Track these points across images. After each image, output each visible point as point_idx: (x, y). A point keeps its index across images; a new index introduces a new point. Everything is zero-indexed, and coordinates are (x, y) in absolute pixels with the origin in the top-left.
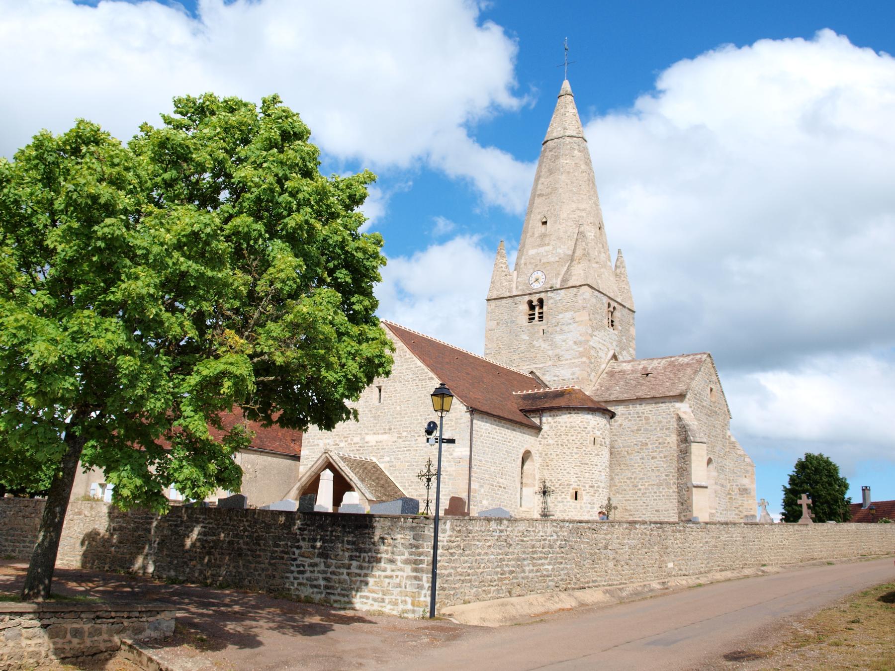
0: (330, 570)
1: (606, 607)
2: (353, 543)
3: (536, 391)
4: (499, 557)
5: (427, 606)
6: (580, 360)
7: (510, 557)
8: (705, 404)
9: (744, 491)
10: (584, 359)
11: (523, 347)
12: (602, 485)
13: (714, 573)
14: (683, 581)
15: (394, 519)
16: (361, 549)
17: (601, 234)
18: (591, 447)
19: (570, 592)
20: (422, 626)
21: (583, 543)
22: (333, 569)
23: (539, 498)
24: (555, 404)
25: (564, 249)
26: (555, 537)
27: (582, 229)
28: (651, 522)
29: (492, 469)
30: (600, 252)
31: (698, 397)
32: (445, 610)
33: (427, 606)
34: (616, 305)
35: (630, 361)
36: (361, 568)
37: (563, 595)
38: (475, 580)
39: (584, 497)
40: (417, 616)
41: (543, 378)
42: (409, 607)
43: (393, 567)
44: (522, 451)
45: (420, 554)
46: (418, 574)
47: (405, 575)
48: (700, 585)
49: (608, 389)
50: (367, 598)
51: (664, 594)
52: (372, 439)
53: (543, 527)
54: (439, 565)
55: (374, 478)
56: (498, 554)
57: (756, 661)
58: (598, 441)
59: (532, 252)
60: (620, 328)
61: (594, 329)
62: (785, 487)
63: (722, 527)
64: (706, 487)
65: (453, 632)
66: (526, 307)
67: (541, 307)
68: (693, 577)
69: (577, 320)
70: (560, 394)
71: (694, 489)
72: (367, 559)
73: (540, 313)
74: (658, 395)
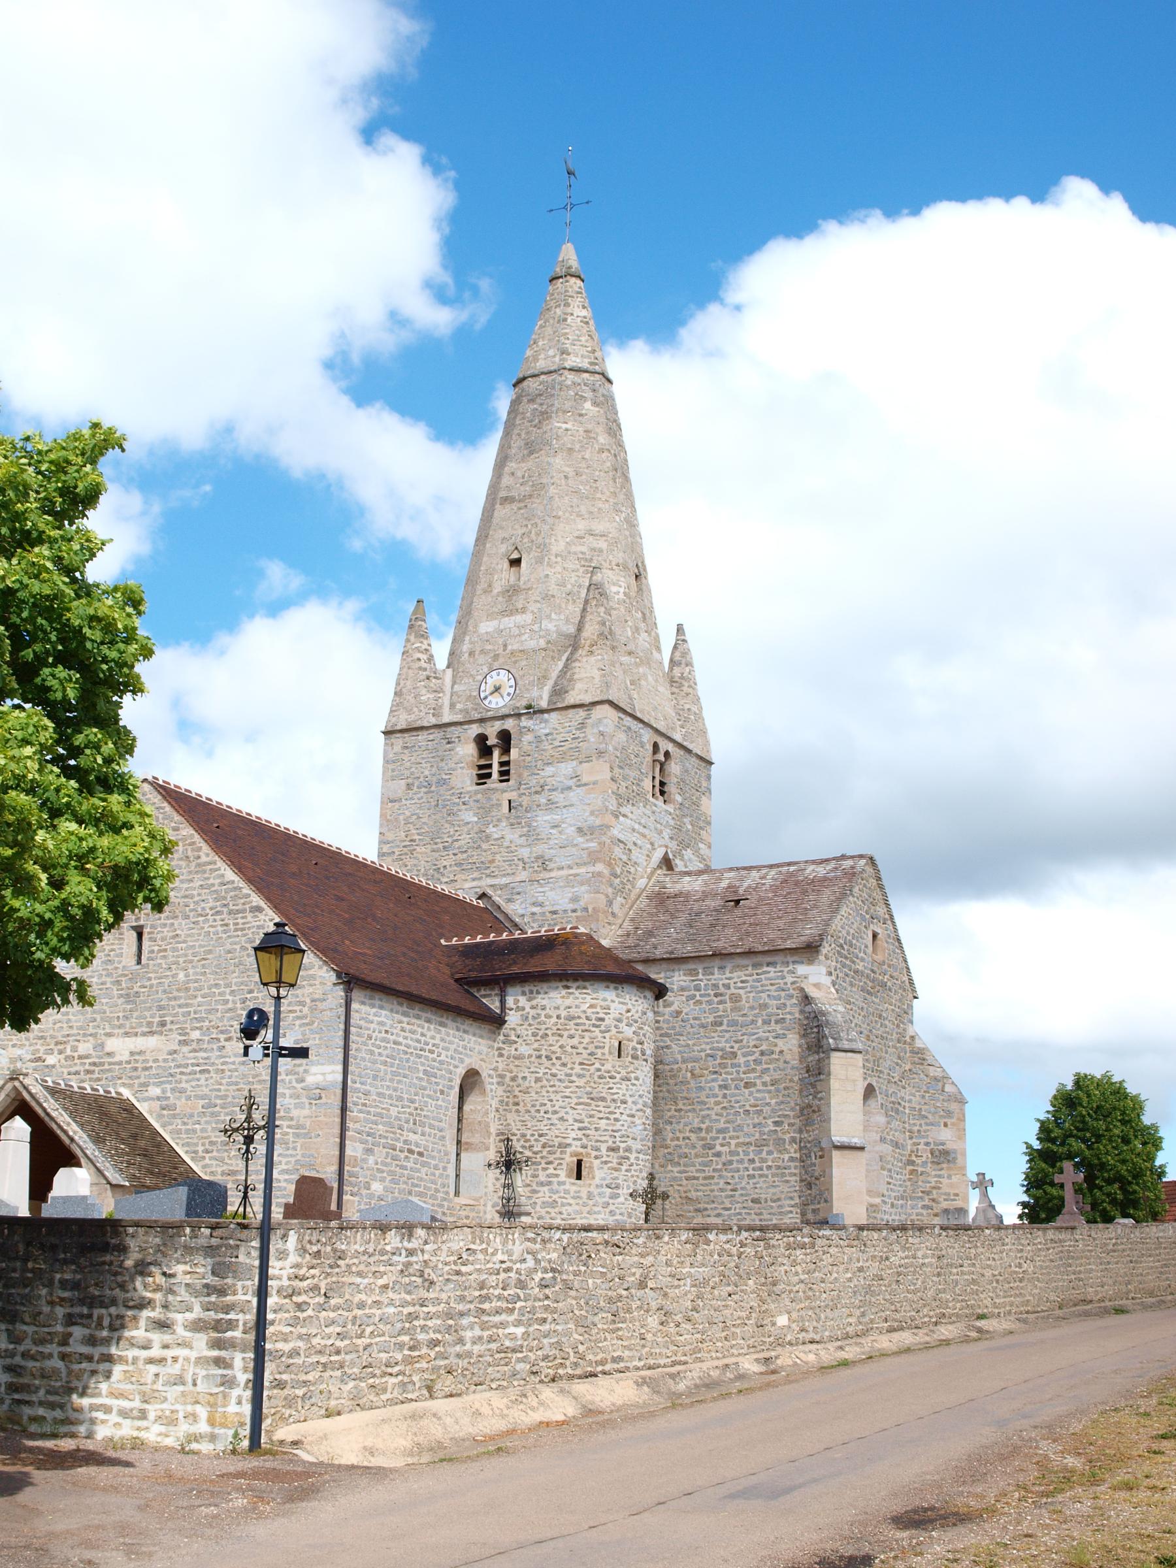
0: (21, 1348)
1: (641, 1416)
2: (76, 1286)
3: (492, 937)
4: (406, 1311)
6: (591, 869)
10: (600, 867)
11: (465, 840)
12: (637, 1146)
13: (874, 1336)
14: (810, 1356)
15: (169, 1229)
16: (94, 1297)
17: (640, 590)
18: (611, 1063)
19: (563, 1384)
20: (232, 1469)
21: (592, 1275)
22: (27, 1345)
23: (493, 1180)
24: (534, 965)
25: (558, 623)
26: (530, 1263)
27: (598, 577)
29: (394, 1111)
30: (637, 630)
31: (846, 952)
32: (285, 1433)
33: (242, 1424)
34: (670, 747)
35: (700, 873)
38: (353, 1364)
39: (598, 1173)
40: (220, 1447)
41: (509, 908)
42: (203, 1427)
44: (461, 1070)
45: (227, 1309)
46: (223, 1353)
47: (193, 1355)
48: (844, 1364)
49: (650, 934)
51: (768, 1385)
54: (270, 1330)
55: (124, 1135)
57: (961, 1529)
58: (628, 1047)
60: (679, 798)
62: (1029, 1146)
64: (862, 1148)
65: (302, 1482)
66: (468, 750)
67: (506, 748)
68: (831, 1346)
69: (585, 780)
70: (545, 945)
71: (836, 1154)
73: (502, 764)
74: (761, 949)
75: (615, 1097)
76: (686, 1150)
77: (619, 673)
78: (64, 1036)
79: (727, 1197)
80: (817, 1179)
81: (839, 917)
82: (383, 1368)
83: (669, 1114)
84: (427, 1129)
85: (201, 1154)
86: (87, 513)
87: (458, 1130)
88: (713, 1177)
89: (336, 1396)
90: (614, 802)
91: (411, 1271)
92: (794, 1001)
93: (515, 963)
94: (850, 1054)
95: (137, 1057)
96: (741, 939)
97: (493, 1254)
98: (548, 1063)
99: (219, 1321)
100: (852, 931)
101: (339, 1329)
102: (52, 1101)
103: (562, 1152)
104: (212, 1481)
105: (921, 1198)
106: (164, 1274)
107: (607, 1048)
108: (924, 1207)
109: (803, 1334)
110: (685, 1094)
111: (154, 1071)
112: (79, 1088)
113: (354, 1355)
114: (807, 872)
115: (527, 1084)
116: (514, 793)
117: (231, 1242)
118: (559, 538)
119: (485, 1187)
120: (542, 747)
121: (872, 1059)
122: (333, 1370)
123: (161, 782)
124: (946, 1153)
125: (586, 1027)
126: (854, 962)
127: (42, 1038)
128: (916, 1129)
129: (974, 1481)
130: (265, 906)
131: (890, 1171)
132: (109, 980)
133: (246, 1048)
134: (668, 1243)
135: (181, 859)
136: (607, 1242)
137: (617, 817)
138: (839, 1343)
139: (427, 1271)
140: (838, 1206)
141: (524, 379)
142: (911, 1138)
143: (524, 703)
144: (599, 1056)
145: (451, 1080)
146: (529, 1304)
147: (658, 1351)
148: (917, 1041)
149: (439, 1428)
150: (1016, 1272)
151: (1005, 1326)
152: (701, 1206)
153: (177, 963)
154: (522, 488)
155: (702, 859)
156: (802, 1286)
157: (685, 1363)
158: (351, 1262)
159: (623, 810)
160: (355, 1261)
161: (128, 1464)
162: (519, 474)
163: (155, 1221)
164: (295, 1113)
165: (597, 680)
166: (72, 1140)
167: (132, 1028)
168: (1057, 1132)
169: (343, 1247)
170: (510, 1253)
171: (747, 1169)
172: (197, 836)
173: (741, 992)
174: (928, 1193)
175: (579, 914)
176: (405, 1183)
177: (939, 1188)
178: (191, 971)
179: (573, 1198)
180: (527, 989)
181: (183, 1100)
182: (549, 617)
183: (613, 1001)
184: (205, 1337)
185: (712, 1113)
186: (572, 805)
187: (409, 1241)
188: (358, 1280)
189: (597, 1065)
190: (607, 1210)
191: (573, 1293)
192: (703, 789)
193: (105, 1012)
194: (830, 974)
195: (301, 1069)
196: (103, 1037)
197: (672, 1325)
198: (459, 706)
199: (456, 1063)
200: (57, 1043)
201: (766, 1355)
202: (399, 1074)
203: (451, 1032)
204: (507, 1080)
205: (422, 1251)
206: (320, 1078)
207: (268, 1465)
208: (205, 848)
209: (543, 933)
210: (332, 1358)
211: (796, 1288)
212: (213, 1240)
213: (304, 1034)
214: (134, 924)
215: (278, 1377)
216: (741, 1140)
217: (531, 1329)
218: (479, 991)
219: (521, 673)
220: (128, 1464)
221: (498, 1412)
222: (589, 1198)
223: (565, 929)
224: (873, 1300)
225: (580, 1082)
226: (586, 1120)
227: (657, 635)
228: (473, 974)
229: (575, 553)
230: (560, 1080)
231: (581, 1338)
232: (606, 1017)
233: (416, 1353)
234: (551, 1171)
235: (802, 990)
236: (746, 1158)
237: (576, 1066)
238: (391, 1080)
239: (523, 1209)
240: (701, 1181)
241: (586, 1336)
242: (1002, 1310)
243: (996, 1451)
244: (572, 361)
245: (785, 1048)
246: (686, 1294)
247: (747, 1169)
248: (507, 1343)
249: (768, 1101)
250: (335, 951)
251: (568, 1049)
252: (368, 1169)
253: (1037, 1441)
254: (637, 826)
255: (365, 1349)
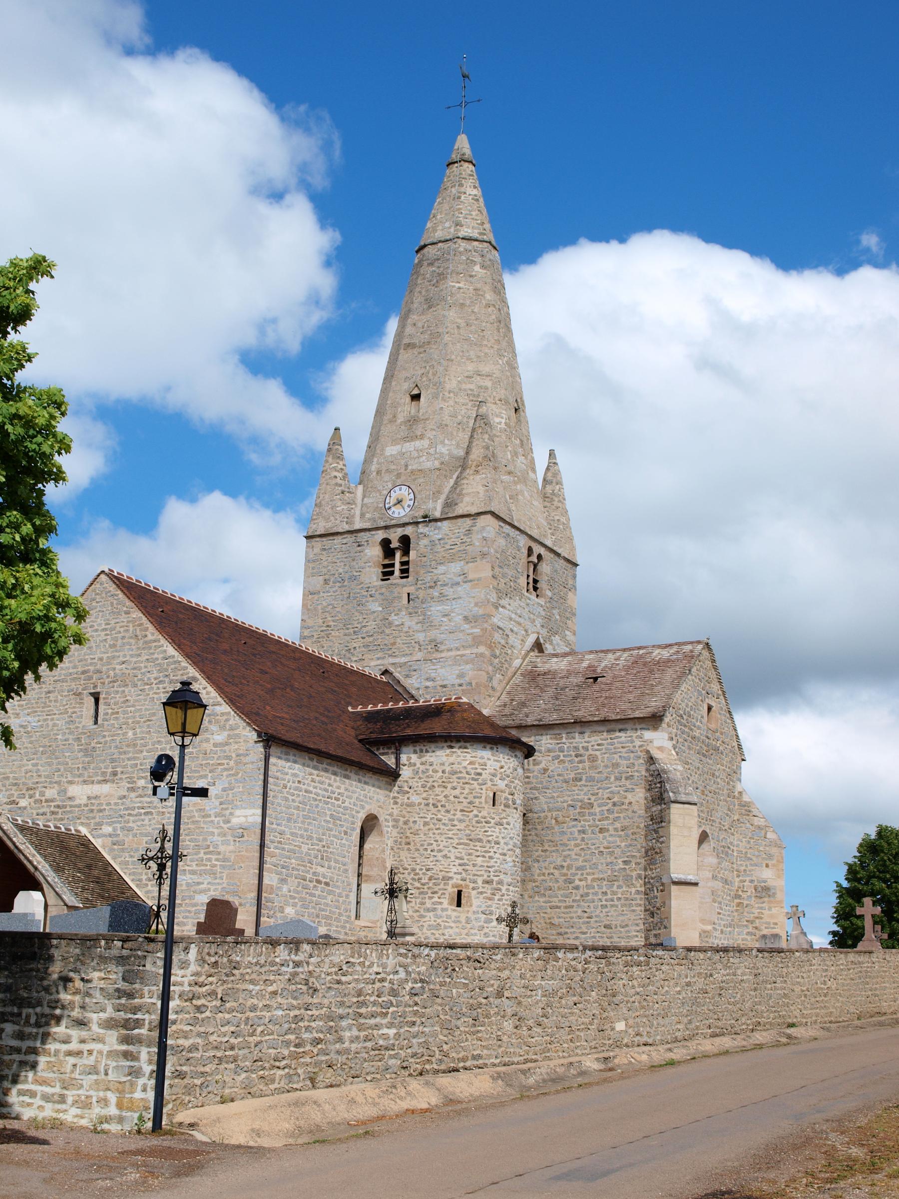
1: (493, 1106)
3: (390, 705)
4: (292, 1014)
5: (147, 1108)
6: (475, 651)
7: (315, 1012)
8: (697, 733)
9: (764, 891)
10: (482, 649)
11: (371, 625)
12: (507, 879)
14: (643, 1056)
15: (87, 941)
17: (519, 421)
19: (429, 1078)
20: (133, 1147)
23: (384, 904)
24: (424, 728)
25: (451, 448)
26: (402, 975)
28: (585, 948)
29: (305, 848)
30: (515, 454)
31: (685, 721)
33: (147, 1108)
34: (542, 551)
35: (565, 655)
36: (20, 1036)
37: (414, 1084)
38: (245, 1058)
39: (475, 902)
40: (127, 1127)
42: (113, 1110)
43: (84, 1034)
44: (362, 816)
45: (135, 1010)
47: (106, 1049)
48: (672, 1063)
49: (523, 704)
50: (33, 1094)
51: (605, 1080)
52: (79, 792)
53: (380, 957)
55: (80, 865)
56: (291, 1008)
59: (391, 450)
60: (549, 594)
61: (502, 594)
62: (839, 885)
63: (717, 957)
64: (696, 884)
66: (375, 552)
67: (406, 551)
68: (661, 1048)
69: (471, 576)
70: (435, 712)
72: (33, 1020)
74: (614, 717)
75: (490, 838)
76: (551, 884)
77: (499, 489)
78: (33, 783)
79: (584, 923)
80: (658, 909)
81: (680, 692)
82: (272, 1062)
83: (537, 854)
84: (332, 864)
85: (144, 882)
86: (18, 328)
87: (359, 865)
88: (572, 907)
89: (229, 1085)
90: (495, 595)
91: (297, 980)
92: (641, 761)
93: (408, 726)
94: (686, 806)
95: (93, 801)
96: (598, 710)
97: (369, 967)
98: (434, 810)
99: (127, 1020)
100: (690, 704)
101: (233, 1029)
102: (21, 836)
103: (445, 884)
104: (113, 1158)
105: (746, 926)
106: (82, 979)
107: (483, 798)
108: (748, 933)
109: (638, 1038)
110: (549, 838)
111: (107, 813)
112: (44, 826)
113: (246, 1051)
114: (654, 654)
115: (417, 827)
116: (413, 588)
117: (139, 953)
118: (452, 378)
119: (376, 909)
120: (436, 550)
121: (706, 810)
122: (227, 1063)
123: (116, 574)
124: (767, 889)
125: (467, 781)
126: (691, 730)
127: (16, 784)
128: (742, 868)
129: (768, 1168)
130: (199, 677)
131: (720, 903)
132: (71, 737)
133: (155, 789)
134: (522, 960)
135: (131, 638)
136: (469, 958)
137: (497, 608)
138: (669, 1046)
139: (311, 980)
140: (675, 931)
141: (425, 246)
142: (738, 876)
143: (421, 513)
144: (477, 804)
145: (353, 823)
146: (401, 1009)
147: (512, 1050)
148: (744, 796)
149: (319, 1114)
150: (822, 989)
151: (810, 1034)
152: (562, 930)
153: (126, 723)
154: (422, 336)
155: (568, 644)
156: (638, 997)
157: (536, 1061)
158: (245, 971)
159: (502, 602)
160: (248, 970)
161: (44, 1142)
162: (420, 325)
163: (76, 935)
164: (222, 848)
165: (481, 495)
166: (36, 868)
167: (89, 777)
168: (862, 874)
169: (238, 959)
170: (384, 966)
171: (600, 900)
172: (144, 618)
173: (598, 753)
174: (752, 922)
175: (464, 687)
176: (314, 908)
177: (761, 918)
178: (138, 730)
179: (454, 922)
180: (418, 749)
181: (131, 837)
182: (442, 443)
183: (489, 759)
184: (116, 1034)
185: (572, 853)
186: (460, 598)
187: (296, 955)
188: (251, 987)
189: (475, 812)
190: (482, 933)
191: (439, 1001)
192: (569, 586)
193: (67, 764)
194: (672, 739)
195: (227, 812)
196: (66, 785)
197: (525, 1028)
198: (368, 516)
199: (358, 809)
200: (28, 789)
201: (606, 1055)
202: (309, 818)
203: (354, 783)
204: (401, 823)
205: (308, 963)
206: (243, 820)
207: (165, 1144)
208: (151, 628)
209: (432, 702)
210: (227, 1053)
211: (633, 999)
212: (124, 951)
213: (230, 784)
214: (93, 691)
215: (179, 1068)
216: (596, 876)
217: (402, 1030)
218: (378, 749)
219: (419, 488)
220: (44, 1142)
221: (370, 1100)
222: (467, 923)
223: (450, 699)
224: (699, 1010)
225: (461, 826)
226: (466, 857)
227: (533, 459)
228: (374, 736)
229: (465, 390)
230: (444, 824)
231: (445, 1039)
232: (483, 772)
233: (301, 1050)
234: (436, 899)
235: (648, 752)
236: (600, 891)
237: (458, 813)
238: (303, 822)
239: (407, 930)
240: (563, 910)
241: (450, 1037)
242: (809, 1020)
243: (791, 1141)
244: (464, 232)
245: (632, 800)
246: (537, 1003)
247: (600, 900)
248: (381, 1042)
249: (619, 843)
250: (257, 714)
251: (451, 798)
252: (282, 896)
253: (827, 1133)
254: (513, 616)
255: (256, 1046)
